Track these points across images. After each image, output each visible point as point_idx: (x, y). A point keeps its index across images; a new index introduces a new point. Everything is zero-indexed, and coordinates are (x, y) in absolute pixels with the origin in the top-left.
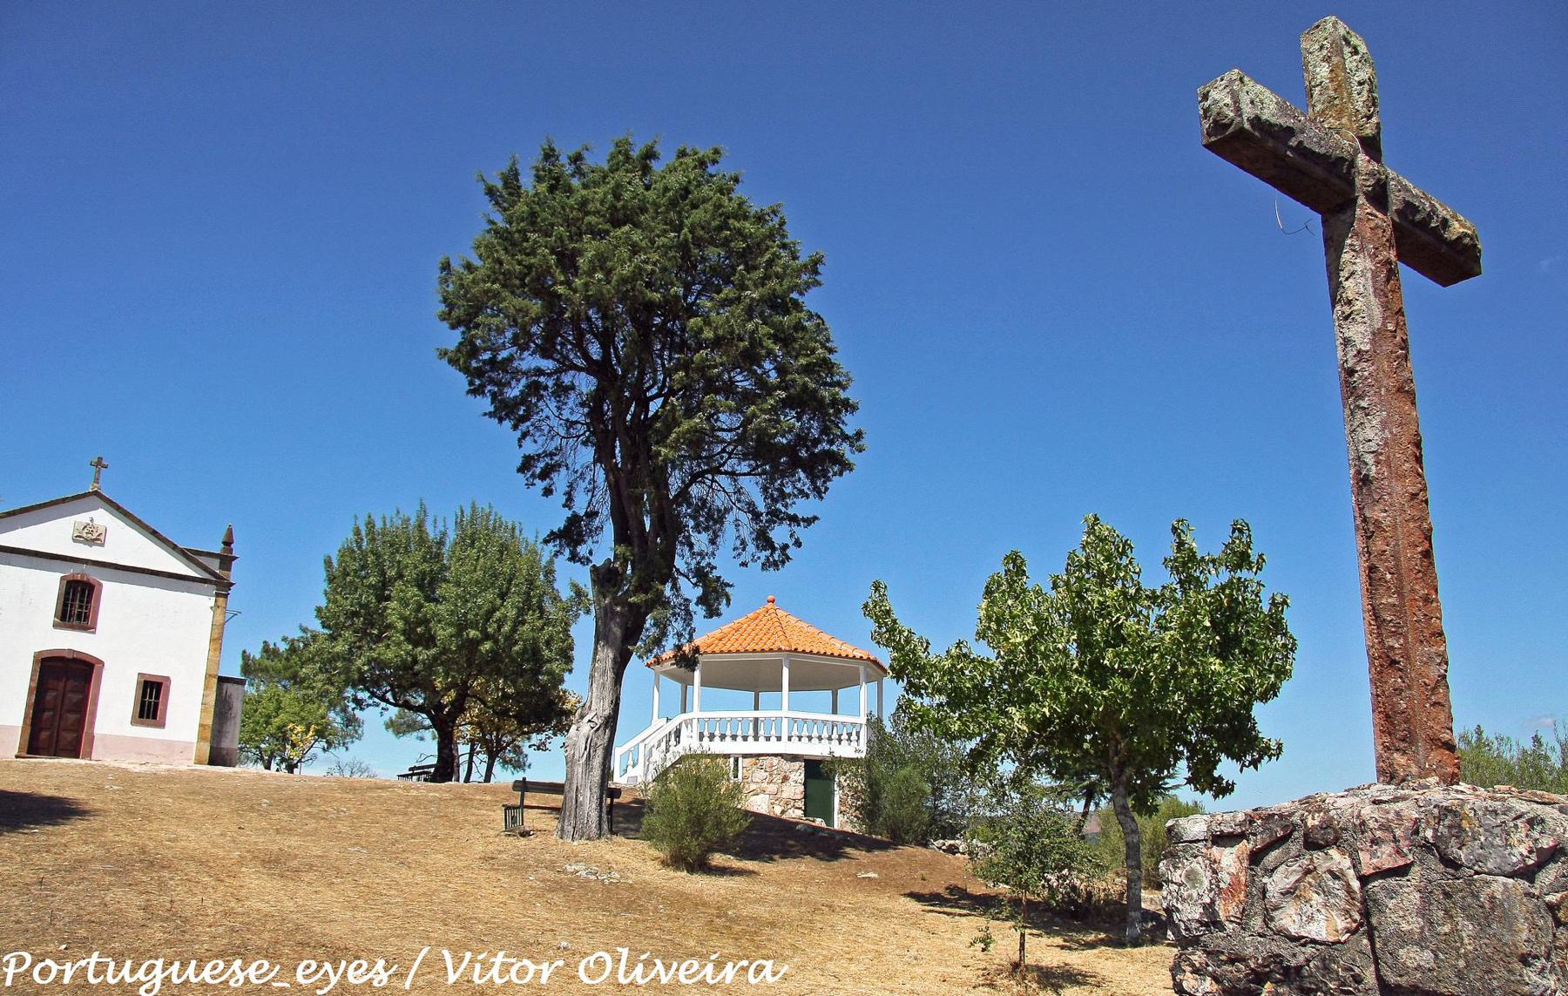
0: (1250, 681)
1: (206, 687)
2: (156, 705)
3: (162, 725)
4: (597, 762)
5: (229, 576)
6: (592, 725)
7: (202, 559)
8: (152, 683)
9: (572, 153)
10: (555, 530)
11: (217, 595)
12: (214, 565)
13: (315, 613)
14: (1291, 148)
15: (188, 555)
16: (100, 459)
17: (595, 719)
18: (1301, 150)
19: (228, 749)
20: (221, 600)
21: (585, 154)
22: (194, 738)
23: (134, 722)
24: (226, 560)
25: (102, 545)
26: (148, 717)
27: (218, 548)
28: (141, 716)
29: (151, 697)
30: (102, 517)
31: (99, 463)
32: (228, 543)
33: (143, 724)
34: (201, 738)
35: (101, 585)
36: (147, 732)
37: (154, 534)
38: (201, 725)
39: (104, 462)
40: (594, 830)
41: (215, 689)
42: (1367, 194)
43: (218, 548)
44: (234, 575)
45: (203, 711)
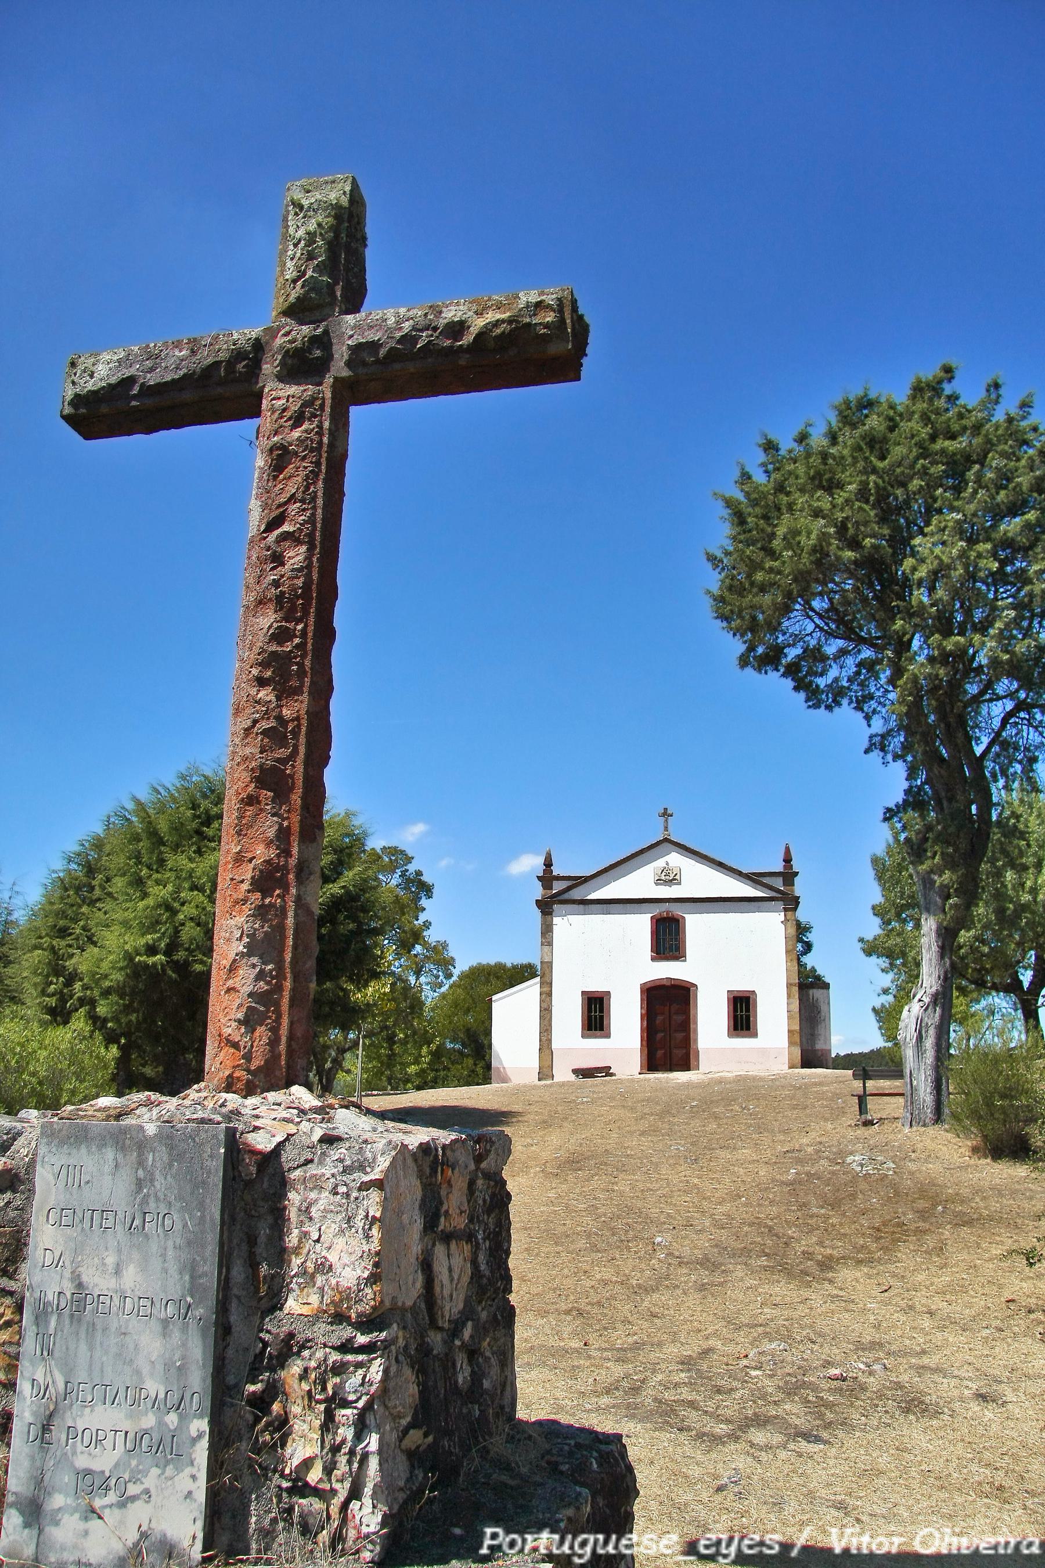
0: (255, 930)
1: (789, 996)
2: (602, 1018)
3: (755, 1035)
4: (929, 1043)
5: (793, 891)
6: (921, 1004)
7: (765, 880)
8: (596, 999)
9: (795, 433)
10: (892, 805)
11: (785, 910)
12: (778, 883)
13: (871, 912)
14: (135, 397)
15: (753, 879)
16: (666, 809)
17: (924, 998)
18: (147, 391)
19: (822, 1050)
20: (789, 913)
21: (810, 430)
22: (785, 1043)
23: (730, 1035)
24: (789, 876)
25: (679, 884)
26: (742, 1029)
27: (779, 867)
28: (736, 1028)
29: (741, 1011)
30: (675, 859)
31: (666, 814)
32: (788, 860)
33: (738, 1036)
34: (791, 1043)
35: (684, 918)
36: (743, 1043)
37: (720, 866)
38: (789, 1031)
39: (669, 812)
40: (929, 1112)
41: (797, 996)
42: (336, 379)
43: (779, 867)
44: (799, 888)
45: (789, 1018)
